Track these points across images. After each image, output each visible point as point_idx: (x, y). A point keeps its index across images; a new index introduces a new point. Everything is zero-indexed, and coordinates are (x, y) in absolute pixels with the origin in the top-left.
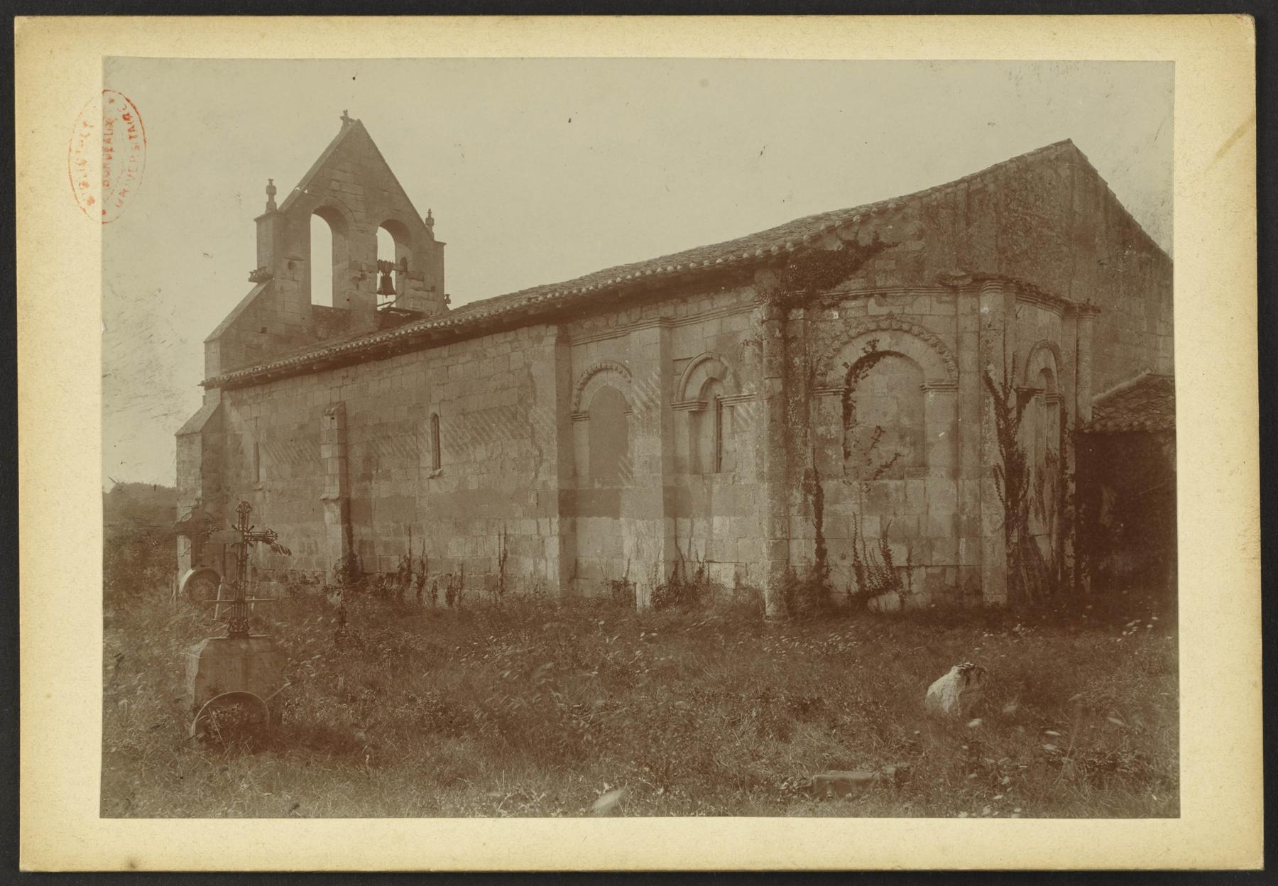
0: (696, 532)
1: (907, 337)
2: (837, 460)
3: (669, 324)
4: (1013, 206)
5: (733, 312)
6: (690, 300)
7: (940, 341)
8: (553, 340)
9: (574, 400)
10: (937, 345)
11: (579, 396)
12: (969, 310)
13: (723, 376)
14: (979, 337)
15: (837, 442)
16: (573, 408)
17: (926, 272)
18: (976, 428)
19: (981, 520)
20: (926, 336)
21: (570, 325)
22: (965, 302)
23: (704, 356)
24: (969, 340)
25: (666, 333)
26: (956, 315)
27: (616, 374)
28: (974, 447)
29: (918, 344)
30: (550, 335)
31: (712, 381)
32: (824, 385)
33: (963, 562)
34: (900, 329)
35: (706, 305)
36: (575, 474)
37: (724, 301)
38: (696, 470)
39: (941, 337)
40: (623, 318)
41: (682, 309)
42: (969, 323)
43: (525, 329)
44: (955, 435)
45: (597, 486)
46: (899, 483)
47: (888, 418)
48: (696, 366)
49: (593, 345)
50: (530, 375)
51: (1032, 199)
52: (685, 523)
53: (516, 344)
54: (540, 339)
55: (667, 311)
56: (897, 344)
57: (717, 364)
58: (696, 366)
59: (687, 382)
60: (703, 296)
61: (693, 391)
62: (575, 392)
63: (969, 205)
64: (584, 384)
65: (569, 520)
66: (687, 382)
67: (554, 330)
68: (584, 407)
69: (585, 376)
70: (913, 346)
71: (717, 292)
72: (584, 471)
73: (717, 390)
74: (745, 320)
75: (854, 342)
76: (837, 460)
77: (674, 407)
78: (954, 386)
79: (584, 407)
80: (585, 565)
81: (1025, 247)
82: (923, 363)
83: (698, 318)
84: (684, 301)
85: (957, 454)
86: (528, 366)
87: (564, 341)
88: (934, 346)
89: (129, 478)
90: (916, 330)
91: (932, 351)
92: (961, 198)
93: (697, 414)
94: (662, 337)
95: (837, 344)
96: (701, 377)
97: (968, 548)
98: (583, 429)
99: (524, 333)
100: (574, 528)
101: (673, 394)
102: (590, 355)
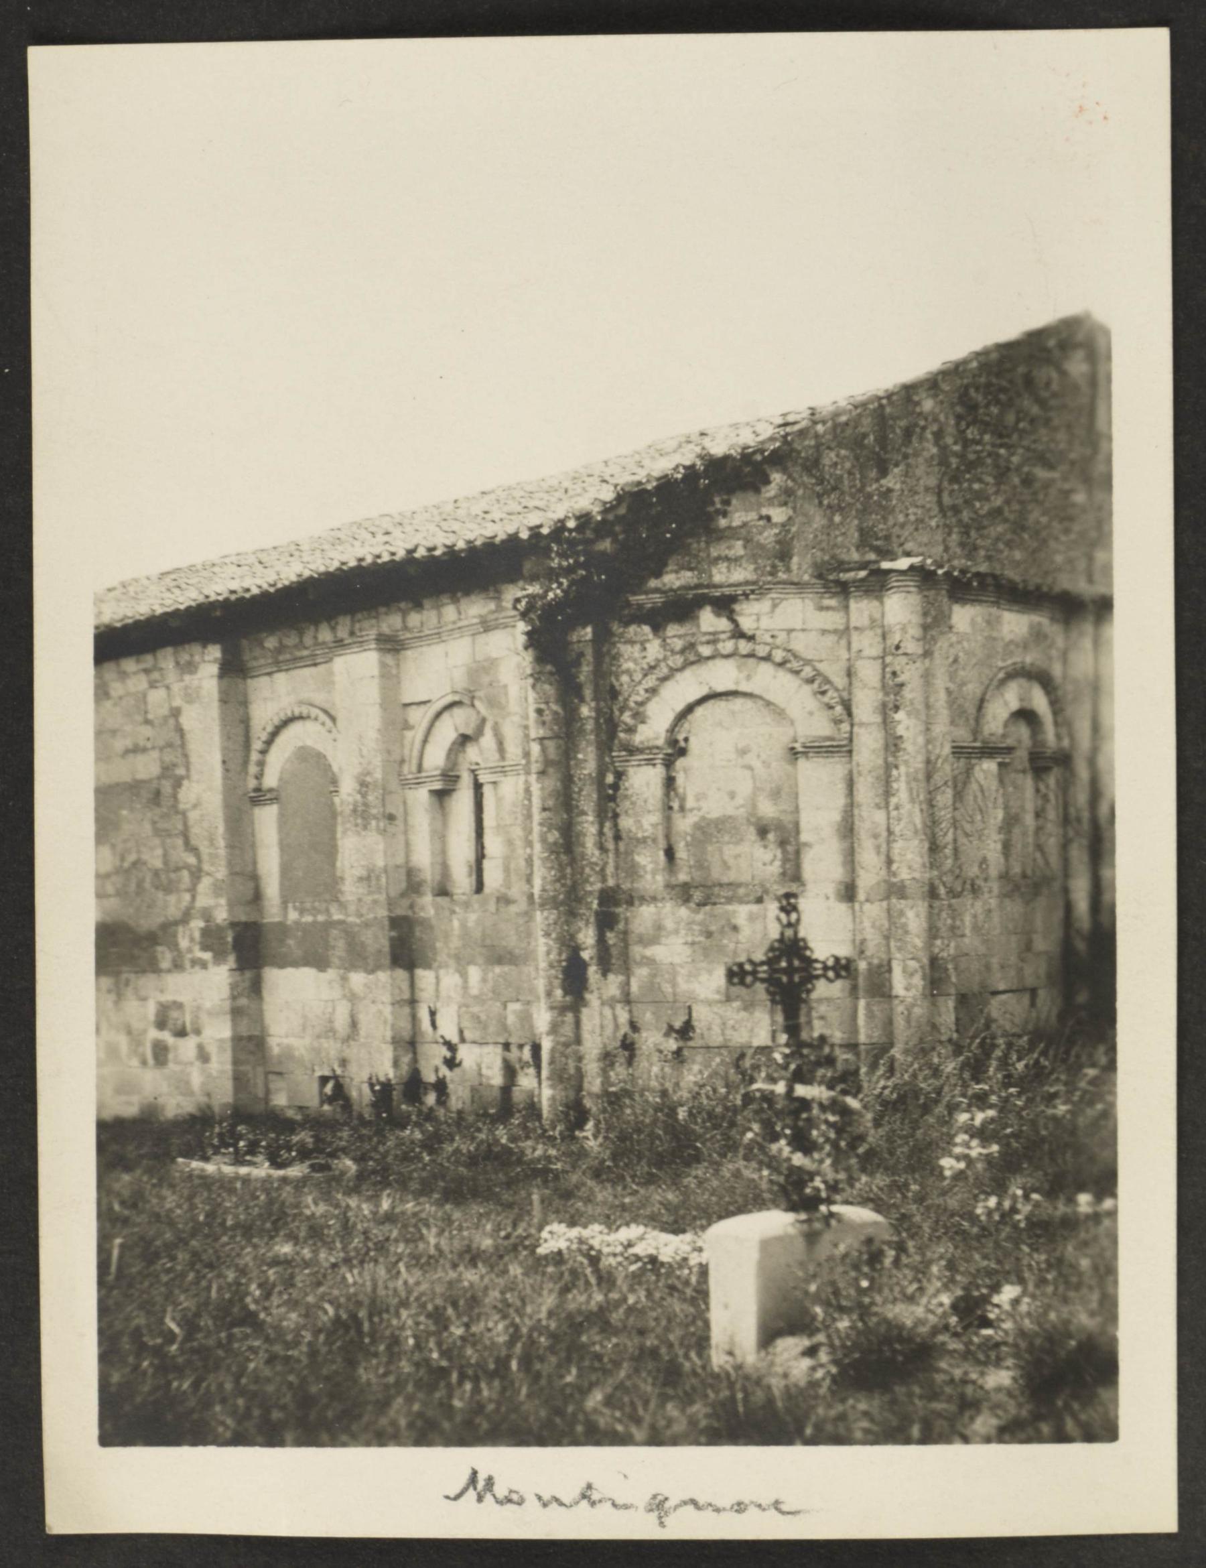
0: (443, 993)
1: (766, 668)
2: (654, 873)
3: (392, 645)
4: (972, 433)
5: (487, 626)
6: (427, 603)
7: (819, 674)
8: (214, 669)
9: (253, 769)
10: (818, 682)
11: (261, 764)
12: (866, 622)
13: (480, 731)
14: (884, 666)
15: (654, 840)
16: (252, 783)
17: (795, 560)
18: (880, 817)
19: (890, 970)
20: (795, 665)
21: (244, 642)
22: (861, 609)
23: (450, 699)
24: (869, 672)
25: (389, 659)
26: (847, 628)
27: (309, 725)
28: (878, 848)
29: (784, 677)
30: (209, 660)
31: (464, 740)
32: (631, 750)
33: (862, 1038)
34: (751, 655)
35: (450, 612)
36: (257, 897)
37: (476, 608)
38: (443, 891)
39: (821, 667)
40: (325, 635)
41: (414, 619)
42: (867, 644)
43: (169, 650)
44: (848, 829)
45: (293, 915)
46: (755, 908)
47: (739, 801)
48: (438, 715)
49: (281, 678)
50: (180, 731)
51: (1010, 418)
52: (425, 977)
53: (155, 675)
54: (190, 668)
55: (391, 622)
56: (749, 678)
57: (470, 711)
58: (438, 715)
59: (425, 741)
60: (445, 599)
61: (436, 758)
62: (254, 756)
63: (882, 440)
64: (269, 743)
65: (248, 974)
66: (425, 741)
67: (215, 652)
68: (271, 780)
69: (270, 729)
70: (768, 680)
71: (467, 593)
72: (272, 889)
73: (472, 753)
74: (480, 654)
75: (678, 676)
76: (654, 873)
77: (405, 784)
78: (844, 749)
79: (271, 780)
80: (276, 1051)
81: (998, 501)
82: (794, 711)
83: (438, 636)
84: (418, 606)
85: (850, 858)
86: (176, 713)
87: (234, 669)
88: (811, 681)
89: (106, 618)
90: (778, 655)
91: (807, 689)
92: (867, 423)
93: (442, 795)
94: (383, 665)
95: (650, 682)
96: (446, 732)
97: (870, 1015)
98: (266, 819)
99: (167, 659)
100: (256, 988)
101: (402, 761)
102: (272, 695)
